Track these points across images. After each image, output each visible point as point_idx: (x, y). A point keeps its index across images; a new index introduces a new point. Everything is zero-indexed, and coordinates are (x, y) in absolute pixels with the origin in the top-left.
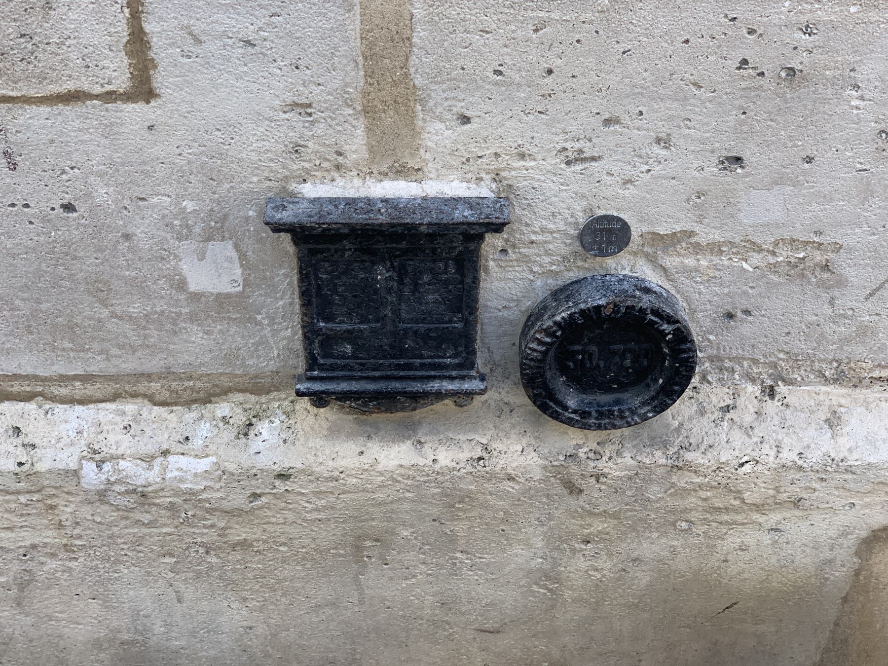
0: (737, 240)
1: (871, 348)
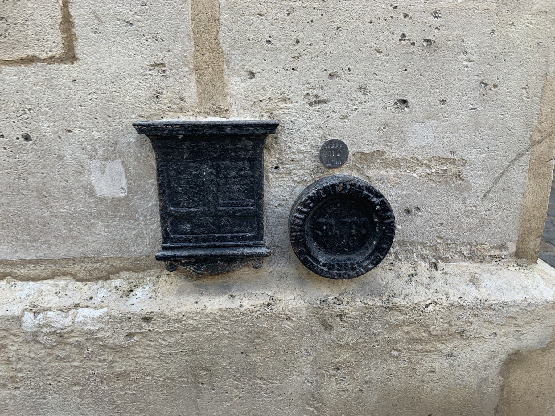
0: (408, 157)
1: (488, 234)
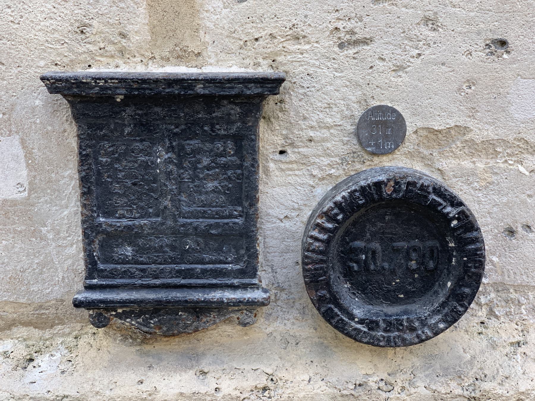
0: (511, 138)
